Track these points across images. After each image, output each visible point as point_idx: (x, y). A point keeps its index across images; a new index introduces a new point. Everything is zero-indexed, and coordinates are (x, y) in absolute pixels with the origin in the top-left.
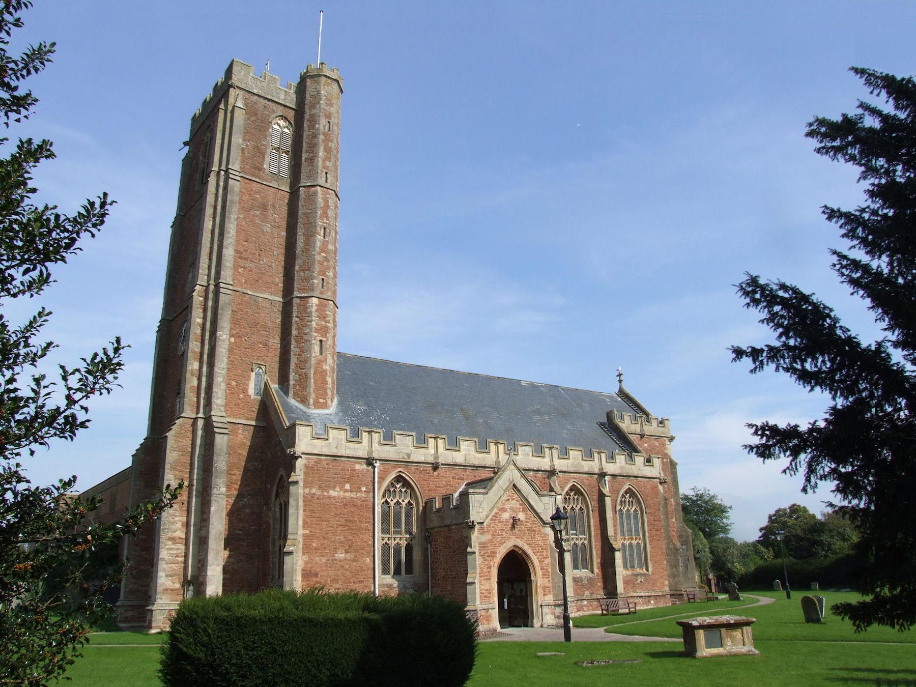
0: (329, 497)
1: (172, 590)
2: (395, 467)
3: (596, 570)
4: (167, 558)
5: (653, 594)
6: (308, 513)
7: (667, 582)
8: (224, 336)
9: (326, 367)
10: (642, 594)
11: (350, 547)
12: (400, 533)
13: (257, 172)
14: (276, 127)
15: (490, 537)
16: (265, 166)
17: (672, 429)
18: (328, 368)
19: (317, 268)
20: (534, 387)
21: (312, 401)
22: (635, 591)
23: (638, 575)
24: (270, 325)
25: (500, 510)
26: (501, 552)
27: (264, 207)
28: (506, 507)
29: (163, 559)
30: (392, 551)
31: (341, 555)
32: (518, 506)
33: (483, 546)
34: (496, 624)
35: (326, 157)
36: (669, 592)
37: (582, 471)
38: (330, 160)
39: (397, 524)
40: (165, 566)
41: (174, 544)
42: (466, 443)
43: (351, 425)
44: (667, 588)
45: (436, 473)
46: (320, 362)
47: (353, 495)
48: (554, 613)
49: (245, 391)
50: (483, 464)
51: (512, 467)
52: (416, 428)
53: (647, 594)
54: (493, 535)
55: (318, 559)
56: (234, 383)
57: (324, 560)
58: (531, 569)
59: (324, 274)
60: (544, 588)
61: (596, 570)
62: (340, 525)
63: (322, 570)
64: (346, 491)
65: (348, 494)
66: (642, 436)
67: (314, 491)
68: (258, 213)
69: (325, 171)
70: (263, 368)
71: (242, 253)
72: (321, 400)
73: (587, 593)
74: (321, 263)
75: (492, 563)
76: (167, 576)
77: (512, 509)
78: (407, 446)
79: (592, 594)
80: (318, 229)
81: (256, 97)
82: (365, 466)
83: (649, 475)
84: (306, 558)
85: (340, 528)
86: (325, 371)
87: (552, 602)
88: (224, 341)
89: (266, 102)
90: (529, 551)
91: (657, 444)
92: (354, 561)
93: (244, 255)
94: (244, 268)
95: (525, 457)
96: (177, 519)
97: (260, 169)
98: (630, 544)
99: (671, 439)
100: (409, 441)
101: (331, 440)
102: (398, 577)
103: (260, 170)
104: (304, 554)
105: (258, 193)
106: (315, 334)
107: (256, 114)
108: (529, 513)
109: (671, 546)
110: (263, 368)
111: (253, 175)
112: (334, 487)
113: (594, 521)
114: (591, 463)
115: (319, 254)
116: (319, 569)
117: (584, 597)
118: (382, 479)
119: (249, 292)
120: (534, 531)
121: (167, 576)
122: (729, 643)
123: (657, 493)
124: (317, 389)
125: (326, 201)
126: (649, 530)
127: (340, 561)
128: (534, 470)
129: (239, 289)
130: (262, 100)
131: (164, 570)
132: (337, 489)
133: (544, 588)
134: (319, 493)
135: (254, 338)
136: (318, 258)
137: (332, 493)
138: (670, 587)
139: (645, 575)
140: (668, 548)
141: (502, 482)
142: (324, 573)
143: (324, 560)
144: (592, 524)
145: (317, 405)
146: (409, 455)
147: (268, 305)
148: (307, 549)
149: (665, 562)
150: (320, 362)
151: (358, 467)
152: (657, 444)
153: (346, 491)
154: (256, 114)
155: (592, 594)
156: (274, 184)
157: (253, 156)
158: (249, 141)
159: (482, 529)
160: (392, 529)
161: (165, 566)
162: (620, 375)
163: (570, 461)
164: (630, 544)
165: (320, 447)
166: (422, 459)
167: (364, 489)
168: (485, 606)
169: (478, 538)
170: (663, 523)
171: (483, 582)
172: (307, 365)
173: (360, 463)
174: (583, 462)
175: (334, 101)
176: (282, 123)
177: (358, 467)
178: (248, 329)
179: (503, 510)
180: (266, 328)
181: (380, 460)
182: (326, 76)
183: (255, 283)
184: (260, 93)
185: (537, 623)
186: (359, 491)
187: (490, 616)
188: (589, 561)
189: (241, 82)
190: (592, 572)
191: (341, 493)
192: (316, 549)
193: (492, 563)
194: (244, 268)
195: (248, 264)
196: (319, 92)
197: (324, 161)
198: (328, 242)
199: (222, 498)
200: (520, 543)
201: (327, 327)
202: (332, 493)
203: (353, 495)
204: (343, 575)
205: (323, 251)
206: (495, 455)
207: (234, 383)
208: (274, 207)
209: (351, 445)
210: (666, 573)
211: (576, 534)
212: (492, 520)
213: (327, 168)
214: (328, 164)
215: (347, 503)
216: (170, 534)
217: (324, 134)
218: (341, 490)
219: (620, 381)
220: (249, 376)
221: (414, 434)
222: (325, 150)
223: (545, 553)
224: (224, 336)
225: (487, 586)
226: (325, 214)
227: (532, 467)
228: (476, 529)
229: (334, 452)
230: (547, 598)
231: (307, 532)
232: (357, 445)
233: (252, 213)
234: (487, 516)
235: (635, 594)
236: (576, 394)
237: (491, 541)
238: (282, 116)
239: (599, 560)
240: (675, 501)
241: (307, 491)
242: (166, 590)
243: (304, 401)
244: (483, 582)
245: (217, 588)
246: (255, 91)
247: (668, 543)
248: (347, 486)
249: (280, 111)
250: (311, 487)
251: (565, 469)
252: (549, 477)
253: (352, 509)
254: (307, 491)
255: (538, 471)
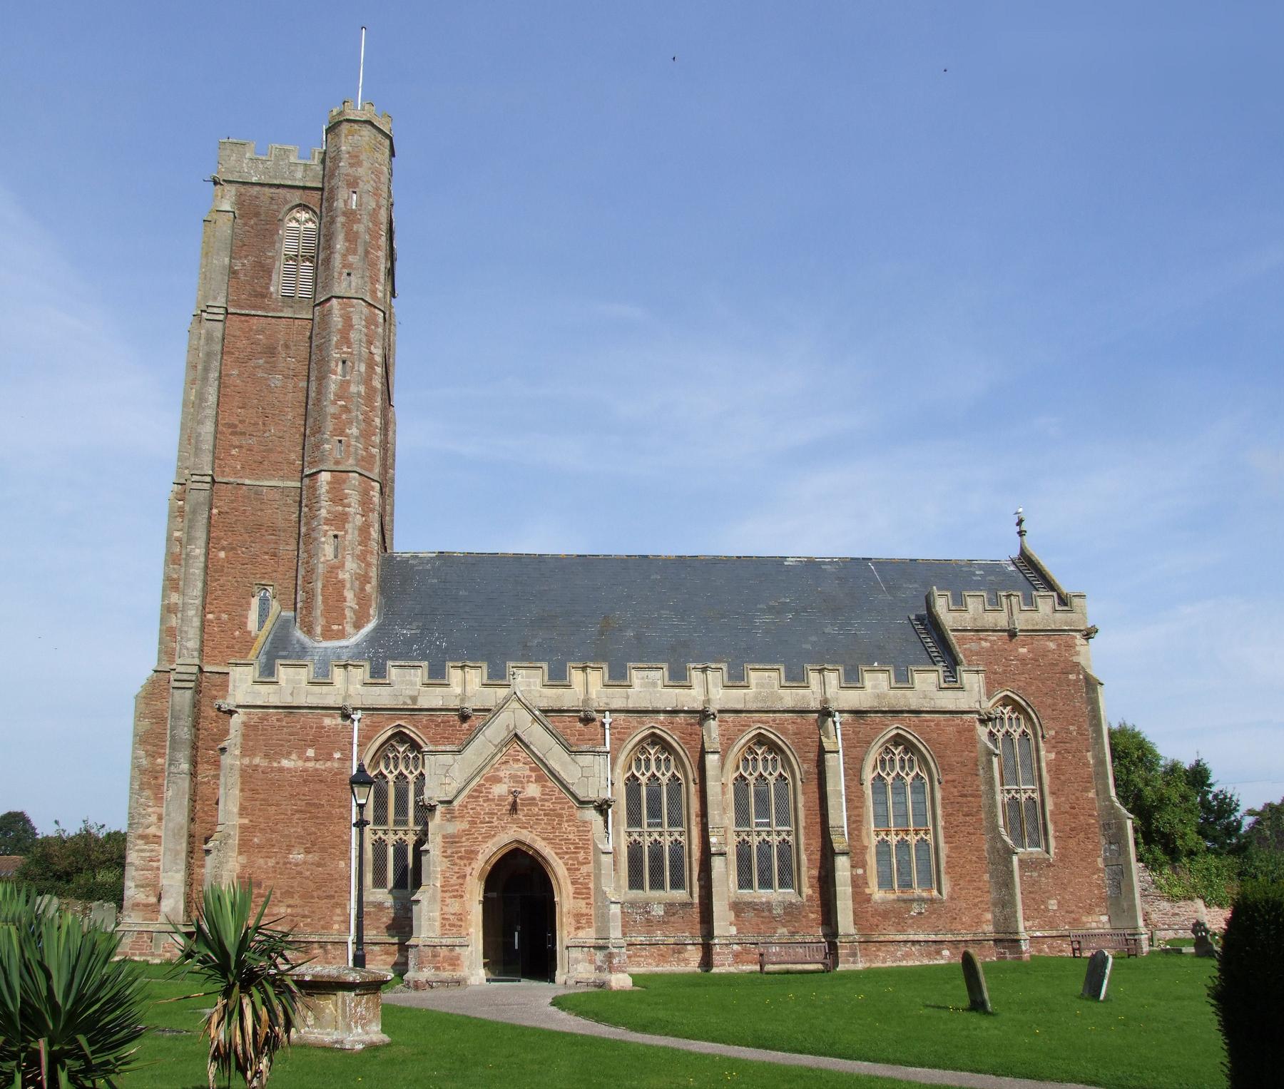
0: (281, 770)
1: (146, 905)
2: (392, 719)
3: (807, 891)
4: (137, 862)
5: (949, 937)
6: (248, 794)
7: (989, 916)
8: (198, 551)
9: (344, 576)
10: (921, 937)
11: (313, 844)
12: (640, 825)
13: (259, 300)
14: (294, 224)
15: (465, 826)
16: (272, 289)
17: (1091, 611)
18: (347, 576)
19: (330, 425)
20: (811, 565)
21: (318, 630)
22: (902, 931)
23: (913, 900)
24: (280, 523)
25: (487, 780)
26: (489, 851)
27: (271, 351)
28: (501, 774)
29: (132, 864)
30: (391, 850)
31: (297, 856)
32: (528, 773)
33: (451, 840)
34: (476, 973)
35: (348, 249)
36: (993, 936)
37: (779, 706)
38: (355, 252)
39: (655, 812)
40: (134, 873)
41: (146, 843)
42: (523, 672)
43: (370, 659)
44: (989, 928)
45: (466, 726)
46: (333, 569)
47: (319, 765)
48: (591, 962)
49: (242, 626)
50: (556, 706)
51: (516, 705)
52: (488, 658)
53: (933, 937)
54: (473, 823)
55: (261, 861)
56: (225, 616)
57: (271, 862)
58: (554, 882)
59: (342, 433)
60: (578, 916)
61: (807, 891)
62: (297, 811)
63: (269, 878)
64: (308, 759)
65: (310, 764)
66: (1012, 634)
67: (257, 761)
68: (261, 361)
69: (346, 271)
70: (270, 589)
71: (236, 426)
72: (335, 627)
73: (782, 931)
74: (334, 416)
75: (468, 870)
76: (137, 886)
77: (514, 778)
78: (413, 684)
79: (793, 934)
80: (333, 364)
81: (257, 188)
82: (339, 720)
83: (951, 707)
84: (243, 859)
85: (297, 816)
86: (342, 582)
87: (592, 942)
88: (196, 557)
89: (273, 190)
90: (547, 851)
91: (1052, 645)
92: (319, 865)
93: (241, 428)
94: (240, 447)
95: (529, 682)
96: (150, 810)
97: (264, 295)
98: (903, 844)
99: (1088, 634)
100: (595, 678)
101: (283, 683)
102: (399, 892)
103: (263, 296)
104: (240, 853)
105: (262, 331)
106: (326, 527)
107: (257, 214)
108: (549, 784)
109: (999, 845)
110: (270, 589)
111: (254, 308)
112: (289, 753)
113: (803, 802)
114: (801, 691)
115: (334, 403)
116: (263, 876)
117: (775, 939)
118: (365, 739)
119: (247, 482)
120: (560, 816)
121: (137, 886)
122: (310, 1021)
123: (973, 741)
124: (327, 610)
125: (347, 319)
126: (947, 816)
127: (297, 865)
128: (665, 712)
129: (232, 480)
130: (266, 190)
131: (133, 878)
132: (294, 756)
133: (578, 916)
134: (264, 763)
135: (256, 548)
136: (331, 410)
137: (285, 763)
138: (996, 924)
139: (932, 901)
140: (993, 849)
141: (495, 731)
142: (270, 883)
143: (271, 862)
144: (800, 805)
145: (328, 634)
146: (414, 699)
147: (277, 497)
148: (245, 847)
149: (986, 877)
150: (333, 569)
151: (327, 722)
152: (1052, 645)
153: (308, 759)
154: (257, 214)
155: (793, 934)
156: (287, 313)
157: (253, 277)
158: (246, 257)
159: (450, 812)
160: (645, 821)
161: (134, 873)
162: (1020, 523)
163: (750, 692)
164: (903, 844)
165: (266, 695)
166: (438, 703)
167: (337, 755)
168: (449, 941)
169: (441, 826)
170: (984, 800)
171: (448, 901)
172: (314, 576)
173: (332, 716)
174: (782, 691)
175: (363, 157)
176: (304, 216)
177: (327, 722)
178: (246, 536)
179: (496, 780)
180: (274, 530)
181: (611, 711)
182: (348, 121)
183: (258, 465)
184: (264, 179)
185: (560, 976)
186: (329, 757)
187: (458, 958)
188: (795, 874)
189: (232, 173)
190: (800, 893)
191: (300, 763)
192: (260, 847)
193: (468, 870)
194: (240, 447)
195: (245, 441)
196: (339, 150)
197: (344, 256)
198: (348, 382)
199: (183, 779)
200: (527, 836)
201: (346, 514)
202: (285, 763)
203: (319, 765)
204: (300, 885)
205: (340, 397)
206: (466, 684)
207: (225, 616)
208: (287, 346)
209: (316, 689)
210: (989, 898)
211: (769, 825)
212: (469, 796)
213: (350, 266)
214: (351, 258)
215: (310, 778)
216: (140, 831)
217: (344, 214)
218: (300, 758)
219: (1021, 533)
220: (249, 604)
221: (665, 666)
222: (347, 239)
223: (581, 856)
224: (198, 551)
225: (454, 906)
226: (346, 340)
227: (661, 706)
228: (438, 813)
229: (289, 701)
230: (581, 934)
231: (246, 821)
232: (325, 689)
233: (252, 363)
234: (459, 792)
235: (901, 938)
236: (854, 570)
237: (467, 833)
238: (299, 205)
239: (815, 872)
240: (1094, 757)
241: (246, 761)
242: (138, 905)
243: (309, 631)
244: (448, 901)
245: (177, 902)
246: (254, 180)
247: (993, 838)
248: (311, 753)
249: (296, 197)
250: (253, 755)
251: (740, 706)
252: (701, 724)
253: (318, 786)
254: (246, 761)
255: (675, 712)
